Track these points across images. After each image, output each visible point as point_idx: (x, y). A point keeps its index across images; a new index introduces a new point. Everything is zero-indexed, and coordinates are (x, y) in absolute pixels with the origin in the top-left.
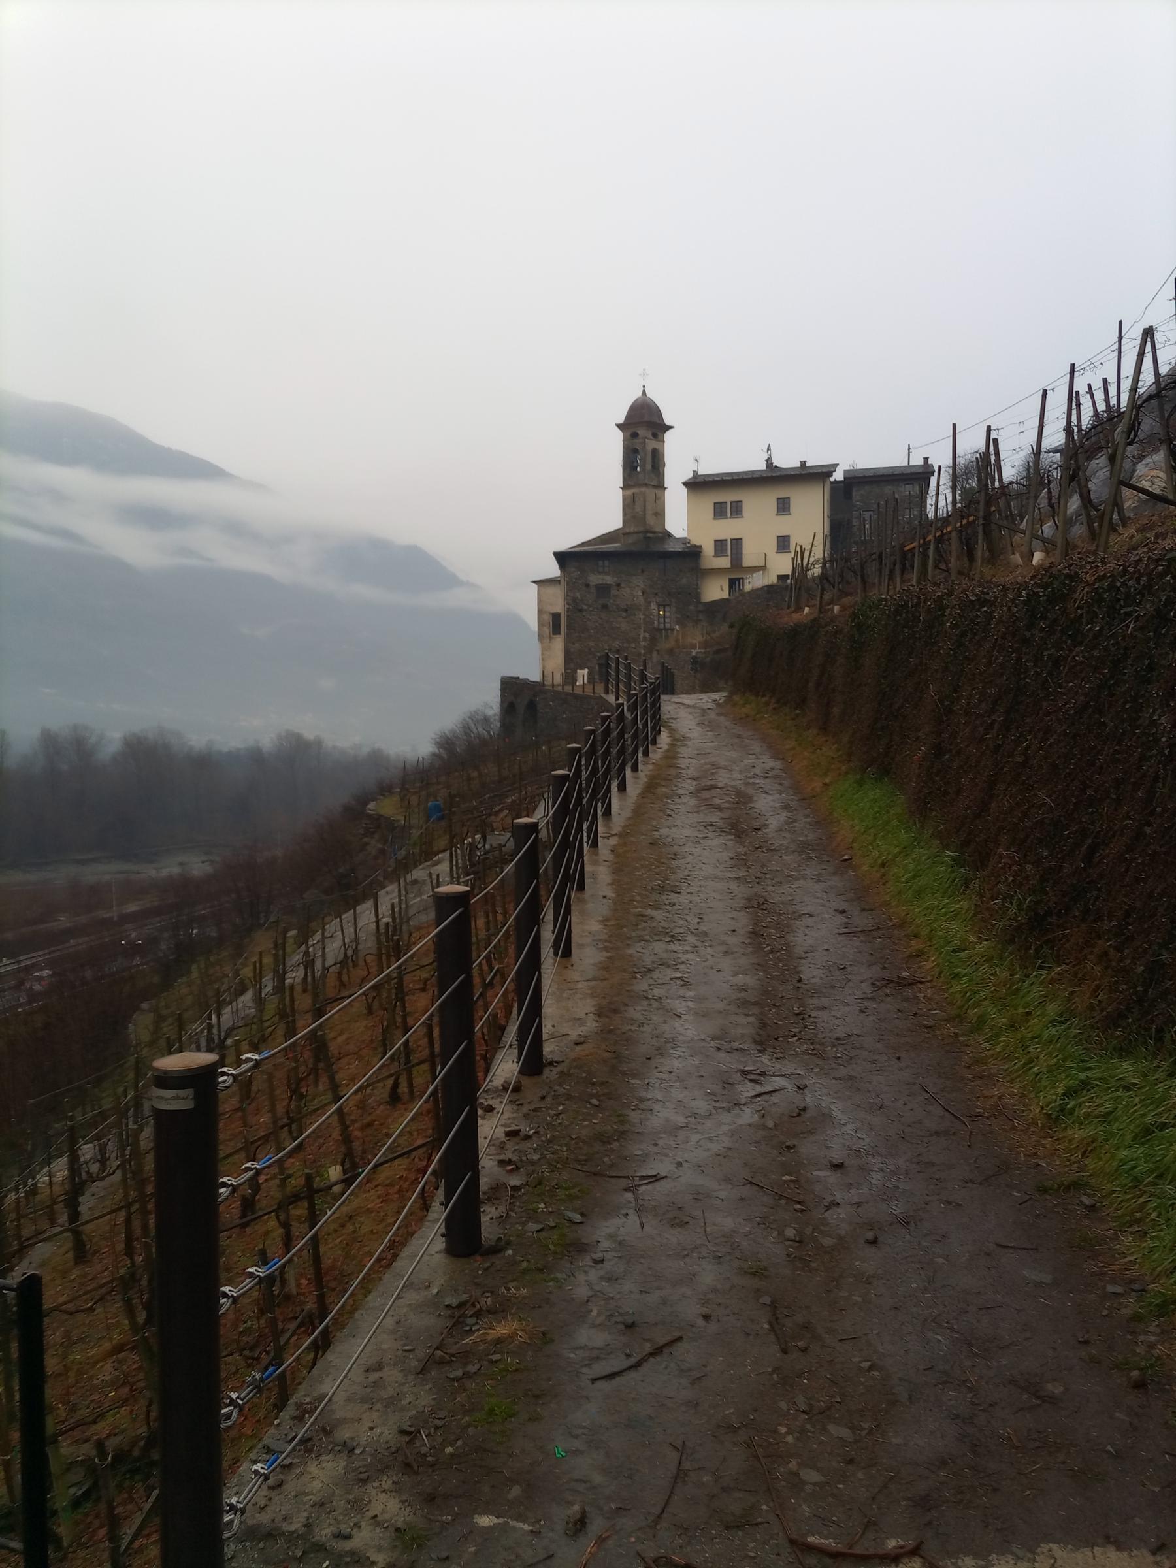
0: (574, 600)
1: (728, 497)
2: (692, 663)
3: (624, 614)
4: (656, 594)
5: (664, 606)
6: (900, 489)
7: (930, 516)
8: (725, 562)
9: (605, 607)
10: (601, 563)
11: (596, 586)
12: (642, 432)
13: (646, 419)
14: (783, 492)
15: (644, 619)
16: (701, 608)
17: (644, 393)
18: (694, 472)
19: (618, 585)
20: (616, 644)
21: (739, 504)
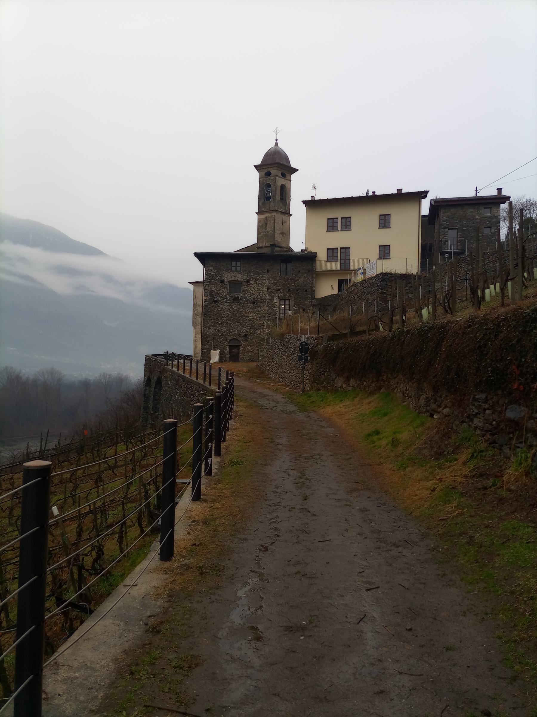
0: (211, 293)
1: (339, 213)
2: (301, 351)
3: (252, 306)
4: (279, 290)
5: (285, 300)
6: (480, 212)
7: (501, 238)
8: (335, 266)
9: (236, 299)
10: (234, 264)
11: (230, 282)
12: (274, 172)
13: (277, 161)
14: (384, 210)
15: (268, 310)
16: (315, 302)
17: (276, 144)
18: (312, 197)
19: (248, 282)
20: (244, 330)
21: (348, 220)
